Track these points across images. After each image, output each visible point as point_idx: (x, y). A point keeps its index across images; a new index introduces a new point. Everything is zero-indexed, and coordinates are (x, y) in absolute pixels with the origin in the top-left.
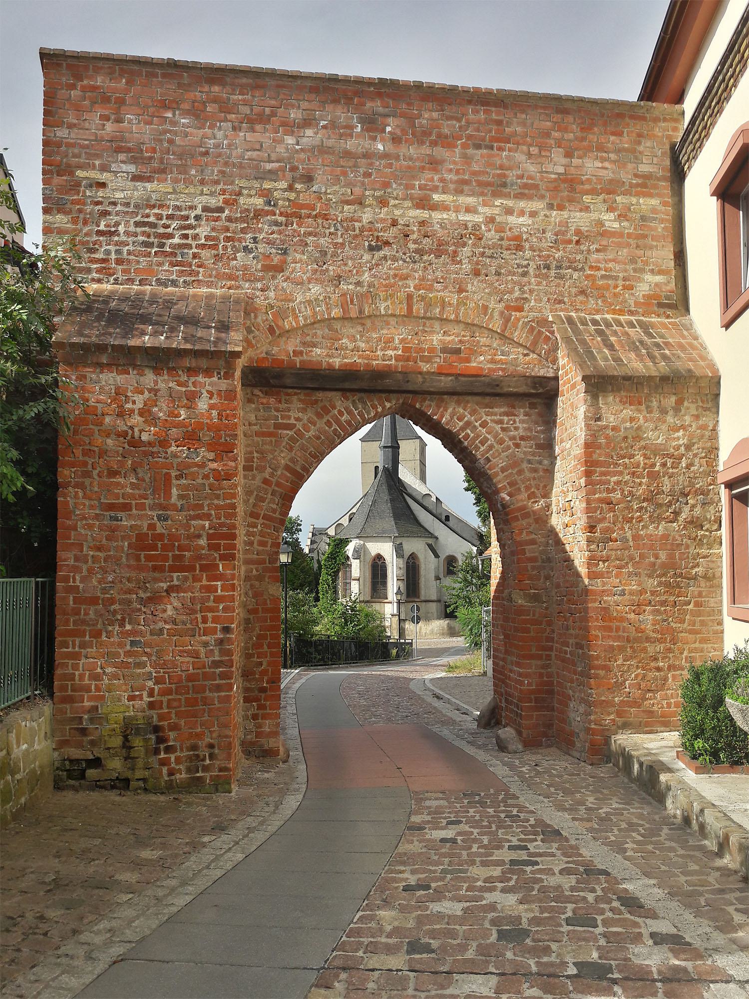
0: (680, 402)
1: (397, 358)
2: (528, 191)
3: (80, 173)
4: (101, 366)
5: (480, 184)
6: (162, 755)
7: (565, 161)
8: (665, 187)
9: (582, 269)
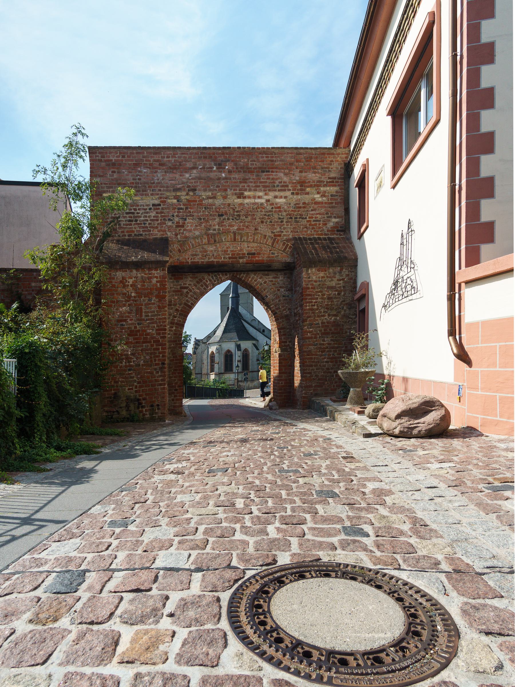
0: (341, 270)
1: (230, 258)
2: (284, 187)
4: (117, 270)
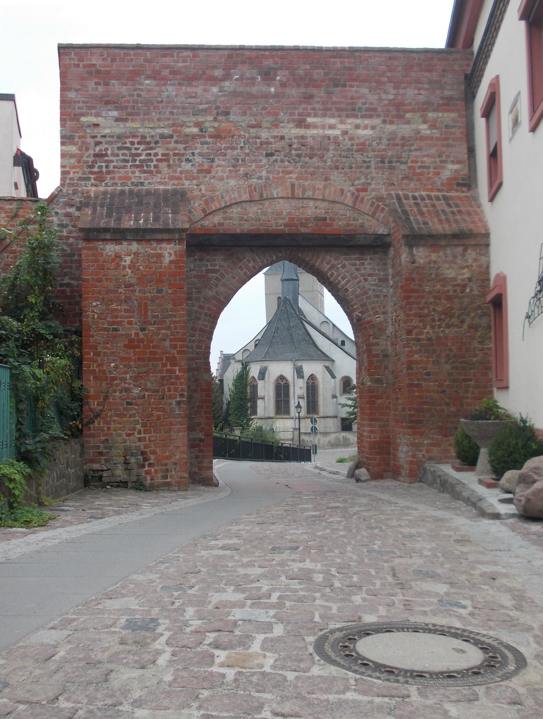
2: (371, 113)
3: (83, 119)
5: (338, 110)
6: (147, 468)
7: (393, 91)
8: (460, 104)
9: (406, 162)
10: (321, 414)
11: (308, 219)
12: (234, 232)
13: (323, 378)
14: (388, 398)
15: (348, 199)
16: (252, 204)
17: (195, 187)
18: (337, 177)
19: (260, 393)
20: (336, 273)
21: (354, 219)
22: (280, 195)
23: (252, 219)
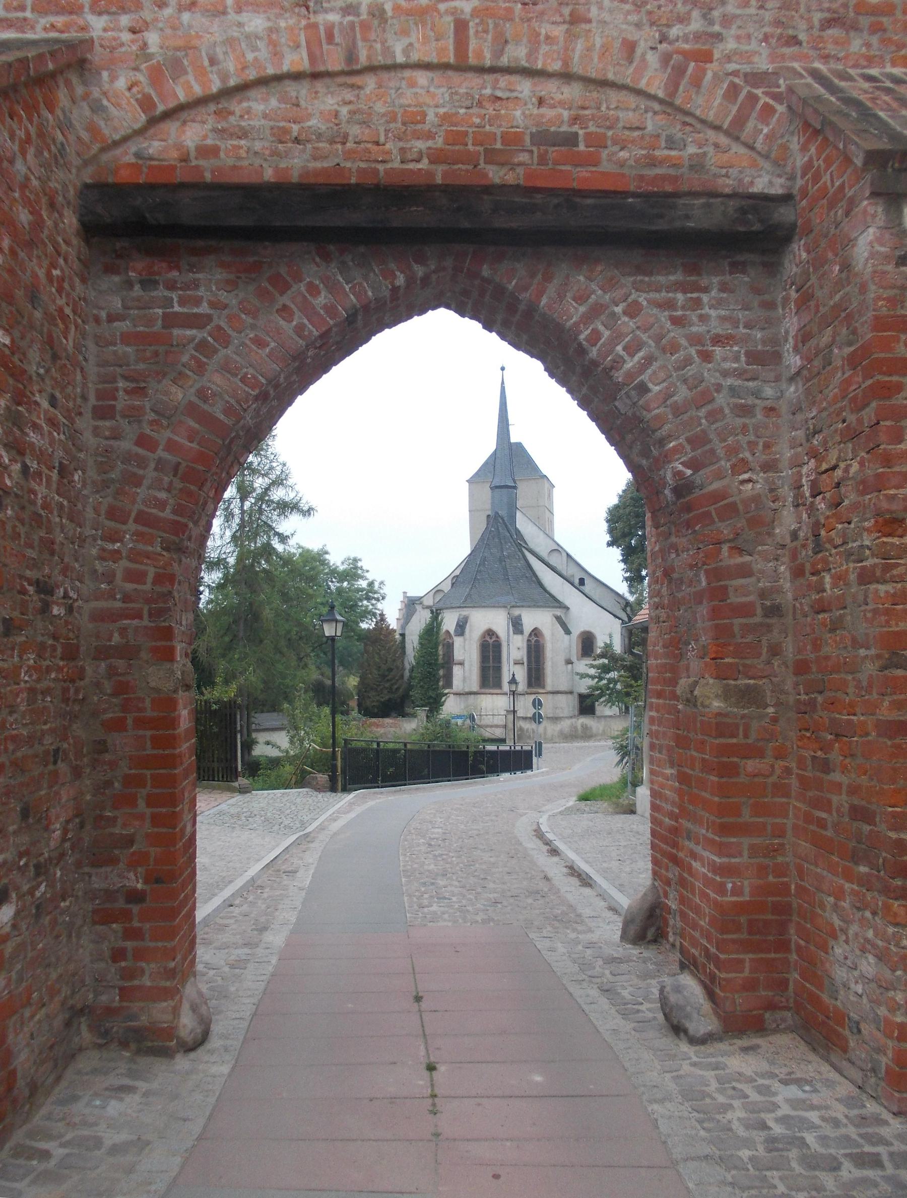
10: (549, 688)
11: (512, 139)
12: (254, 179)
13: (553, 634)
14: (780, 755)
15: (649, 73)
16: (320, 85)
17: (126, 37)
18: (611, 11)
19: (458, 655)
20: (607, 333)
21: (671, 143)
22: (415, 57)
23: (319, 136)
